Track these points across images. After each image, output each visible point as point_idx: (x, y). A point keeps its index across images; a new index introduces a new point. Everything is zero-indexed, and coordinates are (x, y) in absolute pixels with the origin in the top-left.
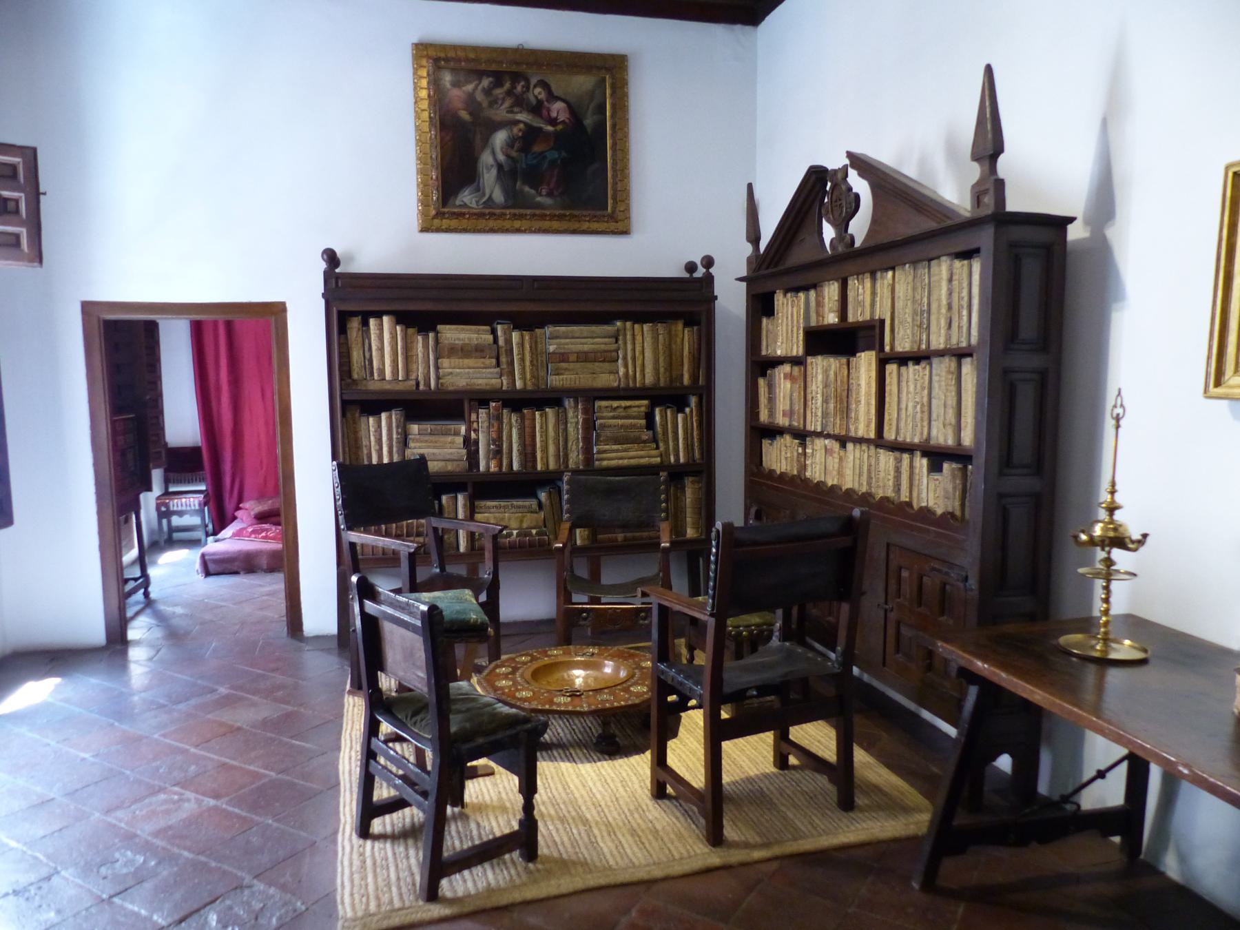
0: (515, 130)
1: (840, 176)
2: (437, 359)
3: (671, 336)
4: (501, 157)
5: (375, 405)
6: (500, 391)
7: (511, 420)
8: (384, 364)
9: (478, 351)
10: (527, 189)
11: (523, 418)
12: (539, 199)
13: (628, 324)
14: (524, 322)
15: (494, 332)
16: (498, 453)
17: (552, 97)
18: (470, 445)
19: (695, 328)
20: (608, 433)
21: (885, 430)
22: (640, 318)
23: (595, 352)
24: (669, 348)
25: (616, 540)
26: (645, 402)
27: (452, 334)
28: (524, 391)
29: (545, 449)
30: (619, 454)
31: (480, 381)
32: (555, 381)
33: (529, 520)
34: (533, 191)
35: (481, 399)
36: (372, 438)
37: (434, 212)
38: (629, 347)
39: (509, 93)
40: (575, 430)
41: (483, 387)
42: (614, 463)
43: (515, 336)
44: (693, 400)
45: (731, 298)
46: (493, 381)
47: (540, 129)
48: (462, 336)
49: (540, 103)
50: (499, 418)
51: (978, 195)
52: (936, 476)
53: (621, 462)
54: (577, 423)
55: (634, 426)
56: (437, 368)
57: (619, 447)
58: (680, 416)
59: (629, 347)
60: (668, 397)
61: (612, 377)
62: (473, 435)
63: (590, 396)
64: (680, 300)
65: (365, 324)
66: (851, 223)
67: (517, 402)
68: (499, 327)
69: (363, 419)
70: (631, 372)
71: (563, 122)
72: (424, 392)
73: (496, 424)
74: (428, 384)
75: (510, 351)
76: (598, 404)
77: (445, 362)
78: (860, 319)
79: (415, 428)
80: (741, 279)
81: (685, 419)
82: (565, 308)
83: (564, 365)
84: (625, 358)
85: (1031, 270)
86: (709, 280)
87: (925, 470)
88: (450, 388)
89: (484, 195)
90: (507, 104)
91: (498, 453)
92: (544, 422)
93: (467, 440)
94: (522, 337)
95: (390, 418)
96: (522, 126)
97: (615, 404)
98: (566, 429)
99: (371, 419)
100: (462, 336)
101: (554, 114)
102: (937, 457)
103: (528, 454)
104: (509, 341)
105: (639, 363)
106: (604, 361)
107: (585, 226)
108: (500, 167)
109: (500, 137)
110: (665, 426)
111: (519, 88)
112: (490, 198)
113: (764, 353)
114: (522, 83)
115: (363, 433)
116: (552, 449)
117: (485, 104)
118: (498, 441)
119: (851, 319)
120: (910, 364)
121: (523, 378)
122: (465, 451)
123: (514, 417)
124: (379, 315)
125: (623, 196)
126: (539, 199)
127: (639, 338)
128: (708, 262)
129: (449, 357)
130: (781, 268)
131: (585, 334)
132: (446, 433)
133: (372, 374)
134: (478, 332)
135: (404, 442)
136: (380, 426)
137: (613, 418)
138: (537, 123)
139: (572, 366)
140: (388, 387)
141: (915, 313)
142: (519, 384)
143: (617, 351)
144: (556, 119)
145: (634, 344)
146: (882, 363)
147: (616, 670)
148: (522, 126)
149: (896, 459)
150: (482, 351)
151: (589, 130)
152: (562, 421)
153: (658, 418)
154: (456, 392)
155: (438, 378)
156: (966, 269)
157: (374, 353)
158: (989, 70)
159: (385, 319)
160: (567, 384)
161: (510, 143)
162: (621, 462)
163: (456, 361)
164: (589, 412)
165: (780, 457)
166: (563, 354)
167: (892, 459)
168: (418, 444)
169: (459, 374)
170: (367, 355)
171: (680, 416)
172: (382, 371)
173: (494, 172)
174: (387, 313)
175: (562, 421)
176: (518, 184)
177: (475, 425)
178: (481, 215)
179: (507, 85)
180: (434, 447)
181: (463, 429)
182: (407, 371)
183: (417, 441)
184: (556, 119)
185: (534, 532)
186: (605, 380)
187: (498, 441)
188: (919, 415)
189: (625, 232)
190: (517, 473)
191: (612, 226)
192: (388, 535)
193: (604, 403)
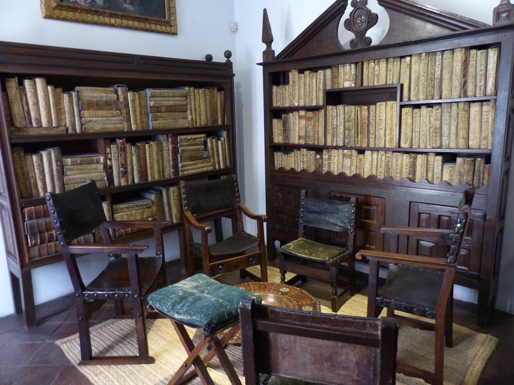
2: (80, 111)
3: (212, 97)
5: (35, 146)
6: (122, 132)
7: (131, 150)
8: (40, 115)
9: (108, 105)
11: (138, 148)
12: (125, 5)
13: (192, 89)
14: (135, 86)
15: (116, 92)
16: (125, 173)
18: (108, 169)
19: (223, 92)
20: (186, 155)
22: (197, 85)
23: (175, 106)
24: (211, 103)
26: (203, 135)
27: (89, 93)
28: (136, 132)
29: (152, 168)
31: (110, 126)
32: (152, 124)
33: (147, 213)
35: (111, 138)
37: (54, 5)
38: (193, 103)
40: (168, 156)
41: (112, 130)
42: (190, 172)
43: (130, 95)
44: (225, 134)
46: (118, 125)
48: (96, 94)
50: (124, 150)
53: (193, 171)
54: (168, 150)
55: (198, 150)
56: (80, 117)
57: (190, 163)
59: (193, 103)
60: (212, 132)
61: (185, 121)
62: (109, 163)
63: (175, 133)
64: (214, 75)
65: (21, 84)
67: (135, 138)
68: (119, 89)
69: (28, 157)
70: (194, 118)
72: (71, 135)
73: (123, 154)
74: (74, 129)
75: (127, 106)
76: (179, 138)
77: (86, 113)
79: (68, 161)
80: (260, 64)
81: (222, 144)
83: (158, 114)
84: (191, 110)
86: (229, 65)
88: (91, 131)
91: (125, 173)
92: (150, 149)
93: (105, 166)
94: (134, 96)
95: (49, 155)
97: (189, 137)
98: (162, 155)
99: (35, 158)
100: (96, 94)
103: (143, 173)
104: (126, 99)
105: (198, 112)
106: (180, 112)
107: (153, 27)
110: (212, 148)
113: (275, 105)
115: (29, 168)
116: (156, 167)
118: (124, 165)
119: (365, 84)
121: (136, 123)
122: (105, 174)
123: (133, 148)
124: (32, 77)
125: (172, 11)
126: (125, 5)
127: (197, 97)
128: (228, 54)
129: (88, 110)
131: (171, 95)
132: (91, 162)
133: (31, 123)
134: (106, 92)
135: (62, 172)
136: (42, 161)
137: (188, 145)
139: (163, 115)
140: (44, 132)
142: (134, 127)
143: (186, 105)
145: (195, 101)
146: (402, 107)
147: (271, 297)
150: (110, 105)
152: (160, 149)
153: (209, 144)
154: (92, 134)
155: (82, 125)
156: (484, 54)
157: (31, 107)
162: (193, 171)
163: (93, 112)
164: (175, 142)
165: (282, 161)
166: (158, 107)
168: (72, 172)
169: (95, 121)
170: (26, 108)
171: (220, 143)
172: (39, 121)
175: (160, 149)
177: (109, 155)
178: (88, 11)
180: (84, 173)
181: (102, 159)
182: (59, 120)
183: (72, 170)
185: (150, 219)
186: (182, 123)
187: (124, 165)
189: (175, 34)
190: (139, 184)
191: (168, 29)
192: (87, 243)
193: (183, 137)
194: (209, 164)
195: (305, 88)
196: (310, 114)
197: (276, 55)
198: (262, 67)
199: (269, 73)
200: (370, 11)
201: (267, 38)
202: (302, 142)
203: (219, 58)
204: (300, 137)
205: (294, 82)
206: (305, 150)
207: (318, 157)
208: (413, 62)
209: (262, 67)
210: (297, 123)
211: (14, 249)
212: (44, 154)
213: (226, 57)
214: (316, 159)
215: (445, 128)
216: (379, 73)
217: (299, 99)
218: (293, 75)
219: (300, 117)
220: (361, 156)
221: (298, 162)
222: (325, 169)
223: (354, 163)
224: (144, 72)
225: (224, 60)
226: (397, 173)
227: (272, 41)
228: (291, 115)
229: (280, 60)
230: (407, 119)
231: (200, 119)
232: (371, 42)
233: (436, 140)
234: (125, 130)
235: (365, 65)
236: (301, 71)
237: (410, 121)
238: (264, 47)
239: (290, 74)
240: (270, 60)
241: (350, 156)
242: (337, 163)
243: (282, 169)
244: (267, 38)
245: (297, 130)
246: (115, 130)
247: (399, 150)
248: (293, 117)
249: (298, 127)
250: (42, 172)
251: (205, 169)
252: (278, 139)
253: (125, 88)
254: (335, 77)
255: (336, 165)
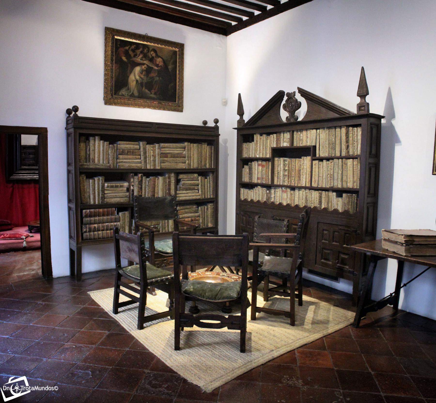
0: (143, 67)
1: (292, 95)
4: (138, 77)
5: (91, 174)
6: (141, 169)
10: (147, 91)
17: (158, 56)
21: (314, 182)
25: (184, 229)
30: (185, 195)
34: (149, 92)
35: (136, 172)
36: (91, 188)
39: (141, 52)
45: (228, 136)
47: (152, 68)
49: (153, 58)
51: (360, 107)
52: (340, 199)
58: (206, 180)
61: (183, 164)
62: (132, 188)
63: (178, 172)
64: (207, 135)
66: (296, 112)
67: (148, 174)
71: (161, 66)
78: (301, 145)
82: (192, 137)
83: (166, 159)
85: (375, 130)
86: (216, 128)
87: (335, 196)
88: (122, 168)
89: (130, 91)
90: (141, 56)
96: (145, 66)
99: (91, 181)
100: (127, 146)
101: (158, 63)
102: (340, 192)
108: (137, 81)
109: (138, 69)
111: (145, 51)
112: (133, 93)
114: (147, 49)
117: (132, 55)
119: (295, 144)
120: (324, 161)
128: (216, 121)
130: (254, 126)
131: (174, 147)
136: (95, 184)
138: (151, 65)
141: (329, 144)
144: (158, 65)
148: (145, 66)
149: (319, 193)
151: (170, 70)
158: (363, 68)
159: (97, 137)
160: (168, 167)
161: (142, 72)
167: (318, 193)
170: (88, 153)
173: (135, 82)
174: (97, 135)
176: (144, 88)
179: (141, 49)
184: (158, 65)
186: (181, 166)
188: (329, 179)
194: (197, 194)
195: (262, 146)
196: (264, 163)
197: (245, 122)
198: (236, 130)
199: (241, 135)
200: (297, 100)
201: (241, 112)
202: (259, 182)
203: (211, 124)
204: (258, 179)
205: (257, 142)
206: (260, 187)
207: (268, 192)
208: (321, 132)
209: (236, 130)
210: (257, 168)
211: (74, 234)
212: (96, 179)
213: (215, 123)
214: (267, 193)
215: (335, 175)
216: (306, 138)
217: (260, 153)
218: (257, 137)
219: (259, 165)
220: (292, 192)
221: (257, 195)
222: (272, 200)
223: (289, 197)
224: (157, 133)
225: (213, 125)
226: (312, 203)
227: (244, 114)
228: (253, 163)
229: (247, 127)
230: (315, 168)
231: (193, 163)
232: (297, 119)
233: (331, 182)
234: (143, 168)
235: (295, 133)
236: (261, 135)
237: (317, 169)
238: (238, 117)
239: (255, 135)
240: (241, 127)
241: (286, 192)
242: (280, 197)
243: (246, 200)
244: (241, 112)
245: (256, 173)
246: (136, 168)
247: (311, 188)
248: (255, 165)
249: (258, 172)
250: (94, 189)
251: (194, 198)
252: (246, 179)
253: (145, 143)
254: (278, 140)
255: (278, 197)
